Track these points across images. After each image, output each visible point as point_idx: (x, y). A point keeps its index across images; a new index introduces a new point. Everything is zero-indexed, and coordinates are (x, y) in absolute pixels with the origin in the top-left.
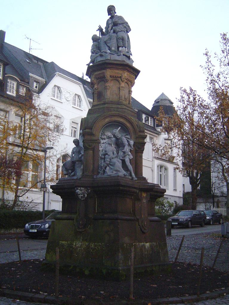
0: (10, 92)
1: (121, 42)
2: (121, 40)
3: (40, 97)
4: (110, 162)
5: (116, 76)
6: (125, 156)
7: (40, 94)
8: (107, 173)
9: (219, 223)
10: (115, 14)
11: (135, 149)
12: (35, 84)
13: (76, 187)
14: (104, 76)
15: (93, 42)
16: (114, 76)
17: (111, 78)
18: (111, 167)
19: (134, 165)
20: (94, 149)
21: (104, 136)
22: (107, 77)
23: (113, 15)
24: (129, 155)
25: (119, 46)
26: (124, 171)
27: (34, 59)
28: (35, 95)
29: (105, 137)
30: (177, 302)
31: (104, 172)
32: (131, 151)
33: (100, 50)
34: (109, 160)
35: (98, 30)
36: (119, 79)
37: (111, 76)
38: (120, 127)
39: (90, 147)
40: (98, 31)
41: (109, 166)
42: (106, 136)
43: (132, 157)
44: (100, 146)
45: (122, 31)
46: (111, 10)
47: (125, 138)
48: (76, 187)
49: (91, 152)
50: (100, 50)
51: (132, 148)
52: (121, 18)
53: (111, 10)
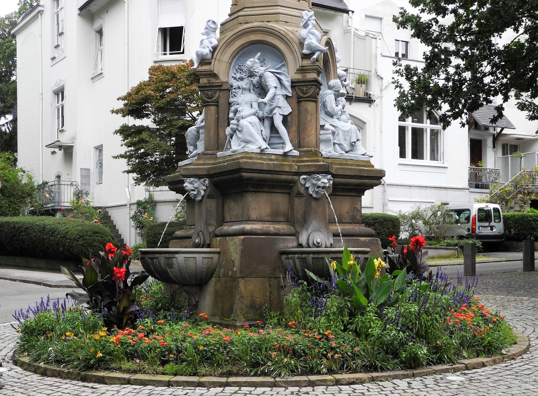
4: (238, 125)
6: (272, 111)
11: (297, 94)
19: (294, 129)
24: (280, 107)
29: (243, 75)
32: (287, 97)
39: (210, 100)
43: (287, 110)
44: (232, 93)
47: (271, 75)
48: (185, 176)
51: (289, 92)
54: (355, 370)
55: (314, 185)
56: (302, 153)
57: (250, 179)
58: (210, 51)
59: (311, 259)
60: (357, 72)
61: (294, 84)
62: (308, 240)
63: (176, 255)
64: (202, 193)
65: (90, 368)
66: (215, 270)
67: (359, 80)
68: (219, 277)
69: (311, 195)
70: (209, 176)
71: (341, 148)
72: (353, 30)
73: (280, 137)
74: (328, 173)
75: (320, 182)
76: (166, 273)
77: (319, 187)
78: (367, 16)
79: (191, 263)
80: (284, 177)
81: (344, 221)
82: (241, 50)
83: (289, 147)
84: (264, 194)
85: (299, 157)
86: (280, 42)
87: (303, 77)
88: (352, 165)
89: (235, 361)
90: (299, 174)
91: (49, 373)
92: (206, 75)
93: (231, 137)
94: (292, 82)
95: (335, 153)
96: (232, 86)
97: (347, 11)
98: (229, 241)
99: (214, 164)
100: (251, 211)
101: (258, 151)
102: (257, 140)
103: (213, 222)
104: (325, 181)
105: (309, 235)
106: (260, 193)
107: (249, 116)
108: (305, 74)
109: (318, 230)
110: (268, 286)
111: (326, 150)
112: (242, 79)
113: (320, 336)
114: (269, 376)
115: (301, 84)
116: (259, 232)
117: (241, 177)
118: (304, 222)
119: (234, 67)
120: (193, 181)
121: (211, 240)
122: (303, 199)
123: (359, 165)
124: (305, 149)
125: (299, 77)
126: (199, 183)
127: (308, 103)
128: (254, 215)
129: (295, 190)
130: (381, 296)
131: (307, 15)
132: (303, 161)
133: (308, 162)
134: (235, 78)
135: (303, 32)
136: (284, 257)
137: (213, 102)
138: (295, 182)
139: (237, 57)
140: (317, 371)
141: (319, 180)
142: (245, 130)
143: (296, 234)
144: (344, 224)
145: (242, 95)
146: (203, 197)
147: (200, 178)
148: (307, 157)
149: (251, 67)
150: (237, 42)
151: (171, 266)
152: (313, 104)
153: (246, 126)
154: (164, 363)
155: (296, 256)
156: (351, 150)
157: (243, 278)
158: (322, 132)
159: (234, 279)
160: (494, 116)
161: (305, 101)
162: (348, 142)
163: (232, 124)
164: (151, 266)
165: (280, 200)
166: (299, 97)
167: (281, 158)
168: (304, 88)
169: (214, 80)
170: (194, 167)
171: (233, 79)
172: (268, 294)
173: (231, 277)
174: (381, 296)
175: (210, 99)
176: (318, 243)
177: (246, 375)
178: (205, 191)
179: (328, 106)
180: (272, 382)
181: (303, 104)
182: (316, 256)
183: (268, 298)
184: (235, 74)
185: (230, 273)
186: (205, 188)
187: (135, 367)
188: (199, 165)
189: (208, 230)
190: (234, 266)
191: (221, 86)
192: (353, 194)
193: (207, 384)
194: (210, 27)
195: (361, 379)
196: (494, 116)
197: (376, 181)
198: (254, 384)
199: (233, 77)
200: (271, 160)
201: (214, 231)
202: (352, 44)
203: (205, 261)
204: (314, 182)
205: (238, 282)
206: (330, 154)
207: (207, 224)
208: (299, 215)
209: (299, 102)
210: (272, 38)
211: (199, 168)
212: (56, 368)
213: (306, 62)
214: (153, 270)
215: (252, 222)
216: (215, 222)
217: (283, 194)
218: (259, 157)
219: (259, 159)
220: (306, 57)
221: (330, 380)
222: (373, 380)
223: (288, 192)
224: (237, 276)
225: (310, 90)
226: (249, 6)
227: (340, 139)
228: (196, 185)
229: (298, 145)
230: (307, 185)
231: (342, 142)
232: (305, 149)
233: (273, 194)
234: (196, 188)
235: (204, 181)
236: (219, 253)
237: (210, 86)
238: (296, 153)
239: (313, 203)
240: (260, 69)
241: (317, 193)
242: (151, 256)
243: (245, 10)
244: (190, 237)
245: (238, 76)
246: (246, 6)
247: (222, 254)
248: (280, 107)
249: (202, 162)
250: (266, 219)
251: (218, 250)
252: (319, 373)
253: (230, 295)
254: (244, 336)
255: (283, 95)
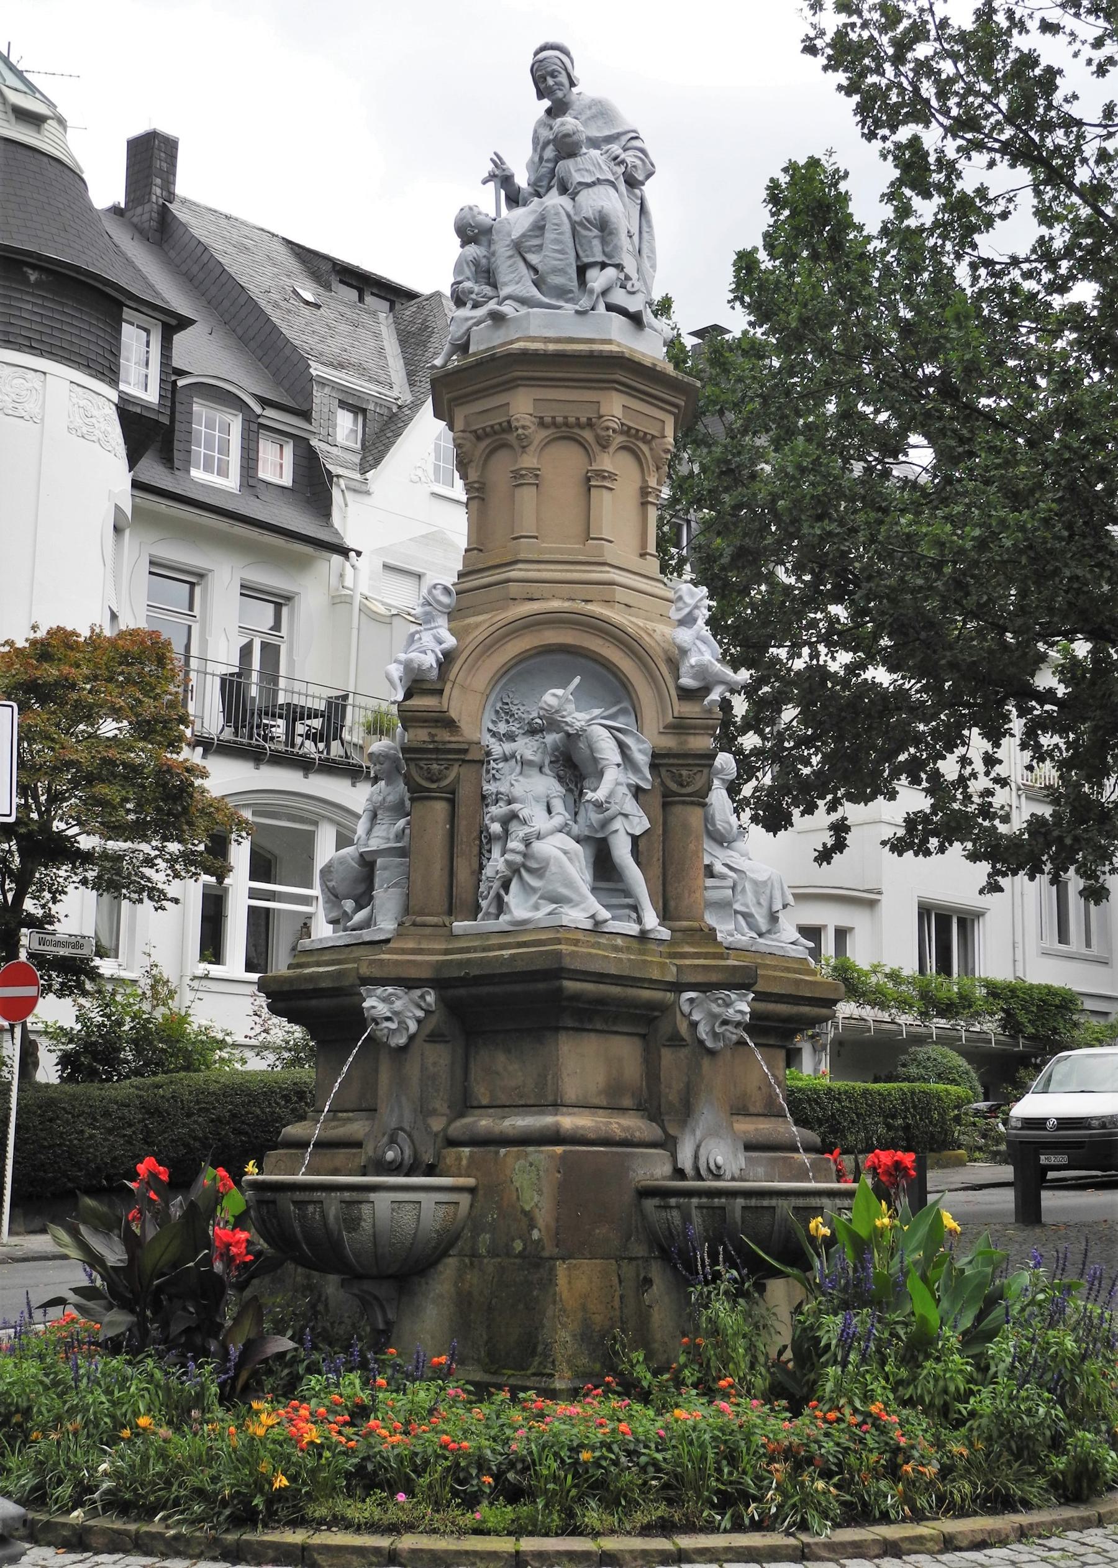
0: (208, 468)
1: (596, 243)
2: (596, 232)
3: (373, 487)
4: (525, 855)
5: (572, 420)
6: (605, 824)
7: (369, 475)
8: (510, 912)
9: (357, 1019)
10: (574, 90)
11: (663, 783)
12: (345, 421)
13: (366, 981)
14: (509, 422)
15: (462, 246)
16: (559, 420)
17: (544, 433)
18: (533, 882)
19: (657, 870)
20: (453, 793)
21: (508, 722)
22: (524, 427)
23: (560, 94)
24: (626, 816)
25: (586, 260)
26: (592, 898)
27: (341, 281)
28: (342, 482)
29: (514, 727)
30: (774, 1554)
31: (501, 906)
32: (637, 792)
33: (495, 286)
34: (521, 847)
35: (492, 177)
36: (587, 435)
37: (542, 424)
38: (577, 680)
39: (434, 786)
40: (491, 185)
41: (521, 877)
42: (520, 720)
43: (640, 823)
44: (488, 772)
45: (599, 182)
46: (550, 77)
47: (605, 733)
48: (366, 981)
49: (440, 808)
50: (495, 286)
51: (645, 779)
52: (601, 111)
53: (550, 77)
54: (962, 1508)
55: (714, 1016)
56: (679, 934)
57: (576, 997)
58: (438, 660)
59: (738, 1213)
60: (372, 704)
61: (657, 761)
62: (696, 1157)
63: (372, 1196)
64: (413, 1027)
65: (246, 1518)
66: (458, 1237)
67: (375, 722)
68: (474, 1255)
69: (701, 1042)
70: (439, 983)
71: (748, 923)
72: (358, 598)
73: (627, 893)
74: (747, 987)
75: (731, 1011)
76: (336, 1245)
77: (725, 1022)
78: (387, 567)
79: (407, 1218)
80: (646, 994)
81: (752, 1110)
82: (516, 664)
83: (651, 919)
84: (593, 1035)
85: (672, 942)
86: (622, 654)
87: (681, 743)
88: (774, 968)
89: (673, 1490)
90: (678, 987)
91: (96, 1541)
92: (425, 721)
93: (506, 886)
94: (654, 755)
95: (739, 936)
96: (488, 754)
97: (344, 552)
98: (510, 1160)
99: (447, 952)
100: (566, 1080)
101: (588, 925)
102: (584, 898)
103: (440, 1104)
104: (742, 1006)
105: (698, 1147)
106: (585, 1034)
107: (552, 833)
108: (684, 737)
109: (713, 1133)
110: (616, 1281)
111: (727, 931)
112: (511, 737)
113: (859, 1418)
114: (771, 1529)
115: (676, 761)
116: (592, 1136)
117: (560, 989)
118: (686, 1111)
119: (493, 706)
120: (391, 994)
121: (438, 1156)
122: (684, 1053)
123: (788, 969)
124: (685, 924)
125: (669, 742)
126: (406, 999)
127: (690, 809)
128: (571, 1090)
129: (664, 1028)
130: (961, 1311)
131: (692, 595)
132: (683, 956)
133: (694, 959)
134: (494, 734)
135: (684, 636)
136: (650, 1204)
137: (440, 790)
138: (666, 1009)
139: (504, 680)
140: (881, 1512)
141: (728, 1004)
142: (553, 868)
143: (669, 1144)
144: (755, 1119)
145: (520, 778)
146: (412, 1038)
147: (410, 988)
148: (691, 944)
149: (557, 712)
150: (509, 646)
151: (353, 1223)
152: (699, 811)
153: (557, 859)
154: (471, 1502)
155: (695, 1201)
156: (769, 932)
157: (563, 1259)
158: (710, 882)
159: (536, 1262)
160: (824, 845)
161: (684, 803)
162: (764, 911)
163: (513, 851)
164: (296, 1224)
165: (625, 1051)
166: (667, 794)
167: (635, 945)
168: (684, 773)
169: (444, 736)
170: (395, 957)
171: (488, 736)
172: (617, 1303)
173: (520, 1255)
174: (961, 1311)
175: (433, 782)
176: (718, 1168)
177: (711, 1528)
178: (419, 1021)
179: (718, 817)
180: (795, 1548)
181: (678, 809)
182: (753, 1202)
183: (618, 1313)
184: (494, 722)
185: (518, 1246)
186: (420, 1014)
187: (392, 1515)
188: (403, 951)
189: (427, 1127)
190: (532, 1225)
191: (466, 751)
192: (772, 1042)
193: (627, 1556)
194: (439, 602)
195: (998, 1532)
196: (824, 845)
197: (825, 1011)
198: (750, 1554)
199: (489, 730)
200: (616, 949)
201: (445, 1130)
202: (355, 632)
203: (441, 1211)
204: (716, 1009)
205: (552, 1270)
206: (731, 939)
207: (424, 1111)
208: (672, 1093)
209: (665, 805)
210: (600, 642)
211: (409, 961)
212: (118, 1525)
213: (689, 709)
214: (300, 1236)
215: (571, 1110)
216: (445, 1105)
217: (625, 1038)
218: (592, 940)
219: (593, 946)
220: (686, 694)
221: (932, 1539)
222: (1022, 1534)
223: (643, 1031)
224: (546, 1254)
225: (698, 777)
226: (531, 557)
227: (747, 901)
228: (398, 1005)
229: (666, 915)
230: (696, 1017)
231: (753, 910)
232: (685, 924)
233: (612, 1037)
234: (396, 1013)
235: (422, 997)
236: (472, 1190)
237: (437, 750)
238: (665, 934)
239: (706, 1062)
240: (577, 718)
241: (715, 1036)
242: (299, 1196)
243: (520, 566)
244: (358, 1145)
245: (502, 728)
246: (522, 556)
247: (481, 1192)
248: (626, 816)
249: (411, 945)
250: (596, 1101)
251: (470, 1181)
252: (885, 1518)
253: (521, 1306)
254: (584, 1421)
255: (629, 786)
